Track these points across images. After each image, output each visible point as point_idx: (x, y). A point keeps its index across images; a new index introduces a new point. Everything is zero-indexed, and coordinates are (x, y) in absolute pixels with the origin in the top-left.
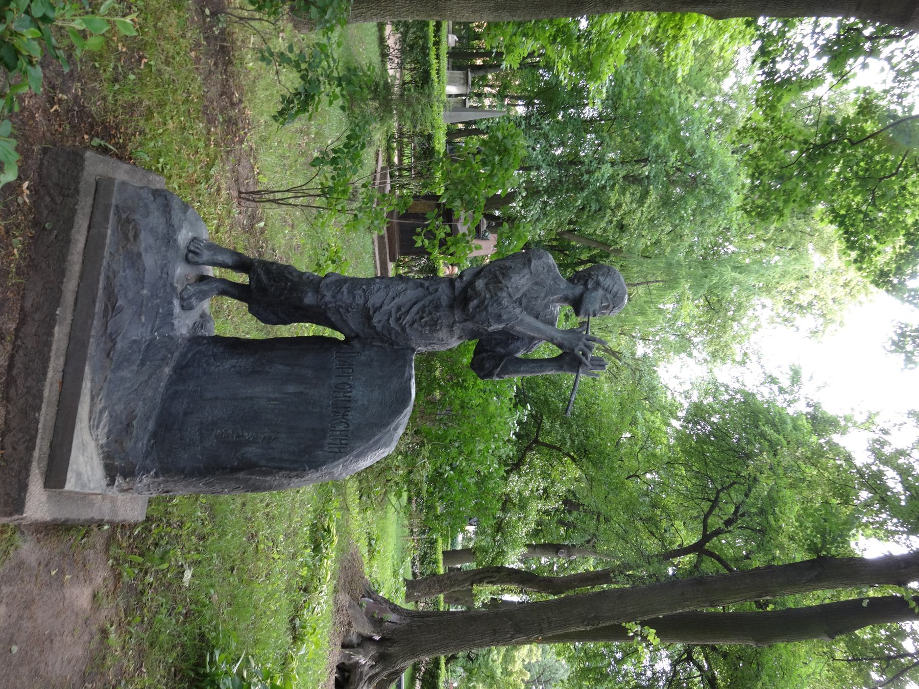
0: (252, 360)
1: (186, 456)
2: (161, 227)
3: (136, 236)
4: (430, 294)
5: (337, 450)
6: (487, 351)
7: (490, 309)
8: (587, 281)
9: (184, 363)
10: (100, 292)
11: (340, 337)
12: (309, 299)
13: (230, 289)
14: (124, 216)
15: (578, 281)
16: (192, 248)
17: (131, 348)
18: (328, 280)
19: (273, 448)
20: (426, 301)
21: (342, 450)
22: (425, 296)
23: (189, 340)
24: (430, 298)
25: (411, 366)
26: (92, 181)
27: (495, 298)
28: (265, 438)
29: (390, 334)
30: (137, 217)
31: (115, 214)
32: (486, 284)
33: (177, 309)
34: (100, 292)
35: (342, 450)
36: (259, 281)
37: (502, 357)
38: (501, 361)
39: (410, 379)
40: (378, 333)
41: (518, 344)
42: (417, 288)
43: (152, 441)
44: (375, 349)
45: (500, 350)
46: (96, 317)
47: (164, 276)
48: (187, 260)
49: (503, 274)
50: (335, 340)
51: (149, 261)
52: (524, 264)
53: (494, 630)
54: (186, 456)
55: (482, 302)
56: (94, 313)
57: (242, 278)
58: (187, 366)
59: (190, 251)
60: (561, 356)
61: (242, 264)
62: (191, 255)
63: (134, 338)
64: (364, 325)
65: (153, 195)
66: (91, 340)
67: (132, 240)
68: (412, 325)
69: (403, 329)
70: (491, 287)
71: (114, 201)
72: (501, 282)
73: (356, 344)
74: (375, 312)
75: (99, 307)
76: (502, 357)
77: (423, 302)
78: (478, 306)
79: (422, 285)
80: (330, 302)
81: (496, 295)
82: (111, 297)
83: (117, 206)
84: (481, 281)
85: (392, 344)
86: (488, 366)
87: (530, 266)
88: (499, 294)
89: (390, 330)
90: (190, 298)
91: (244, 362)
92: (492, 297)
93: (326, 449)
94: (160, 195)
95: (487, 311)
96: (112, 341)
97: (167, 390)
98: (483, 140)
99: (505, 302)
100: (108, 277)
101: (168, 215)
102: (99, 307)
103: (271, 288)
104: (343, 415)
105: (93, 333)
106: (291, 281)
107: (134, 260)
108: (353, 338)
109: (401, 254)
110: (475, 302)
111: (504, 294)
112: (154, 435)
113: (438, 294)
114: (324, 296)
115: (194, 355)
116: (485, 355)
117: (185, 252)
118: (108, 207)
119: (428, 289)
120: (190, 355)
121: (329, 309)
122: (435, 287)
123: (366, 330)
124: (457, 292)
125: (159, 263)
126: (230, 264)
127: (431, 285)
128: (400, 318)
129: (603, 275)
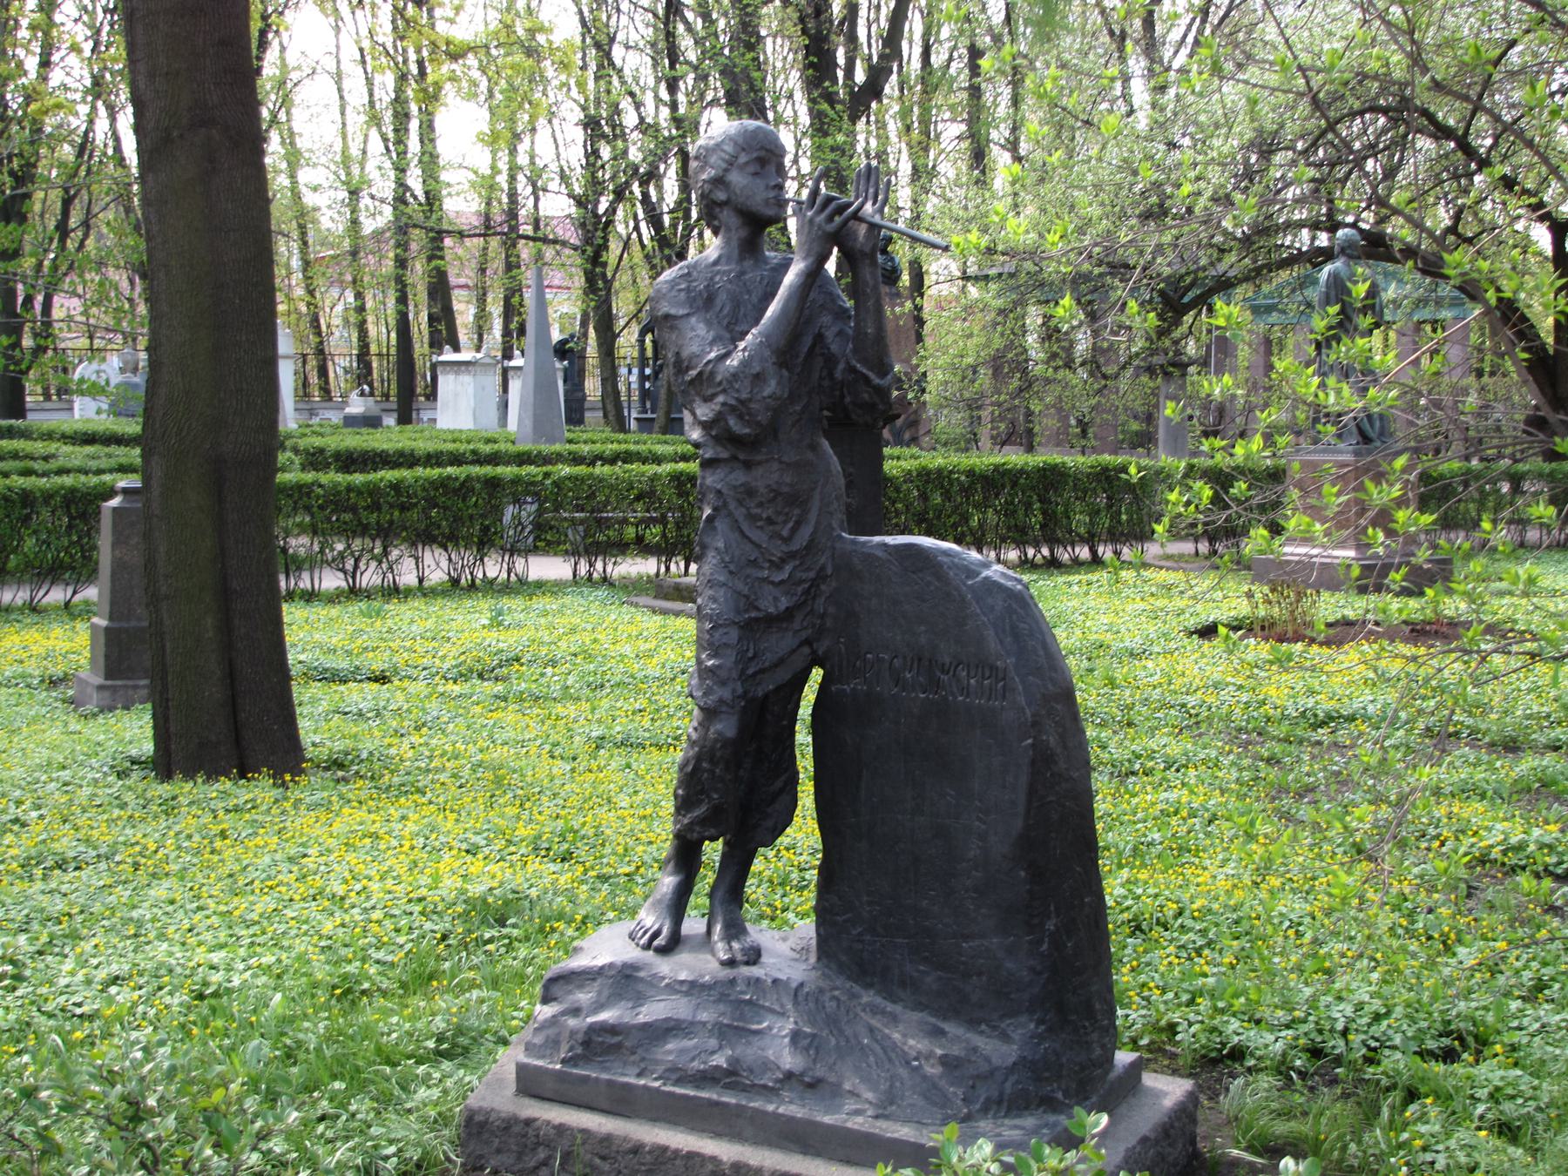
4: (725, 504)
7: (744, 396)
8: (714, 202)
10: (704, 1094)
11: (817, 674)
20: (740, 513)
21: (1001, 675)
22: (730, 514)
24: (732, 505)
25: (864, 543)
29: (802, 581)
31: (575, 1066)
33: (755, 971)
34: (704, 1094)
35: (1001, 675)
39: (885, 545)
42: (715, 529)
43: (983, 1027)
52: (672, 328)
56: (738, 1106)
57: (713, 851)
61: (686, 857)
66: (781, 1110)
69: (792, 555)
74: (758, 609)
75: (729, 1099)
77: (741, 519)
78: (741, 417)
80: (734, 691)
81: (720, 383)
82: (707, 1078)
87: (675, 317)
92: (724, 391)
95: (750, 400)
98: (115, 509)
100: (678, 1082)
102: (729, 1099)
103: (729, 799)
105: (771, 1108)
110: (732, 422)
113: (724, 491)
121: (745, 692)
123: (796, 625)
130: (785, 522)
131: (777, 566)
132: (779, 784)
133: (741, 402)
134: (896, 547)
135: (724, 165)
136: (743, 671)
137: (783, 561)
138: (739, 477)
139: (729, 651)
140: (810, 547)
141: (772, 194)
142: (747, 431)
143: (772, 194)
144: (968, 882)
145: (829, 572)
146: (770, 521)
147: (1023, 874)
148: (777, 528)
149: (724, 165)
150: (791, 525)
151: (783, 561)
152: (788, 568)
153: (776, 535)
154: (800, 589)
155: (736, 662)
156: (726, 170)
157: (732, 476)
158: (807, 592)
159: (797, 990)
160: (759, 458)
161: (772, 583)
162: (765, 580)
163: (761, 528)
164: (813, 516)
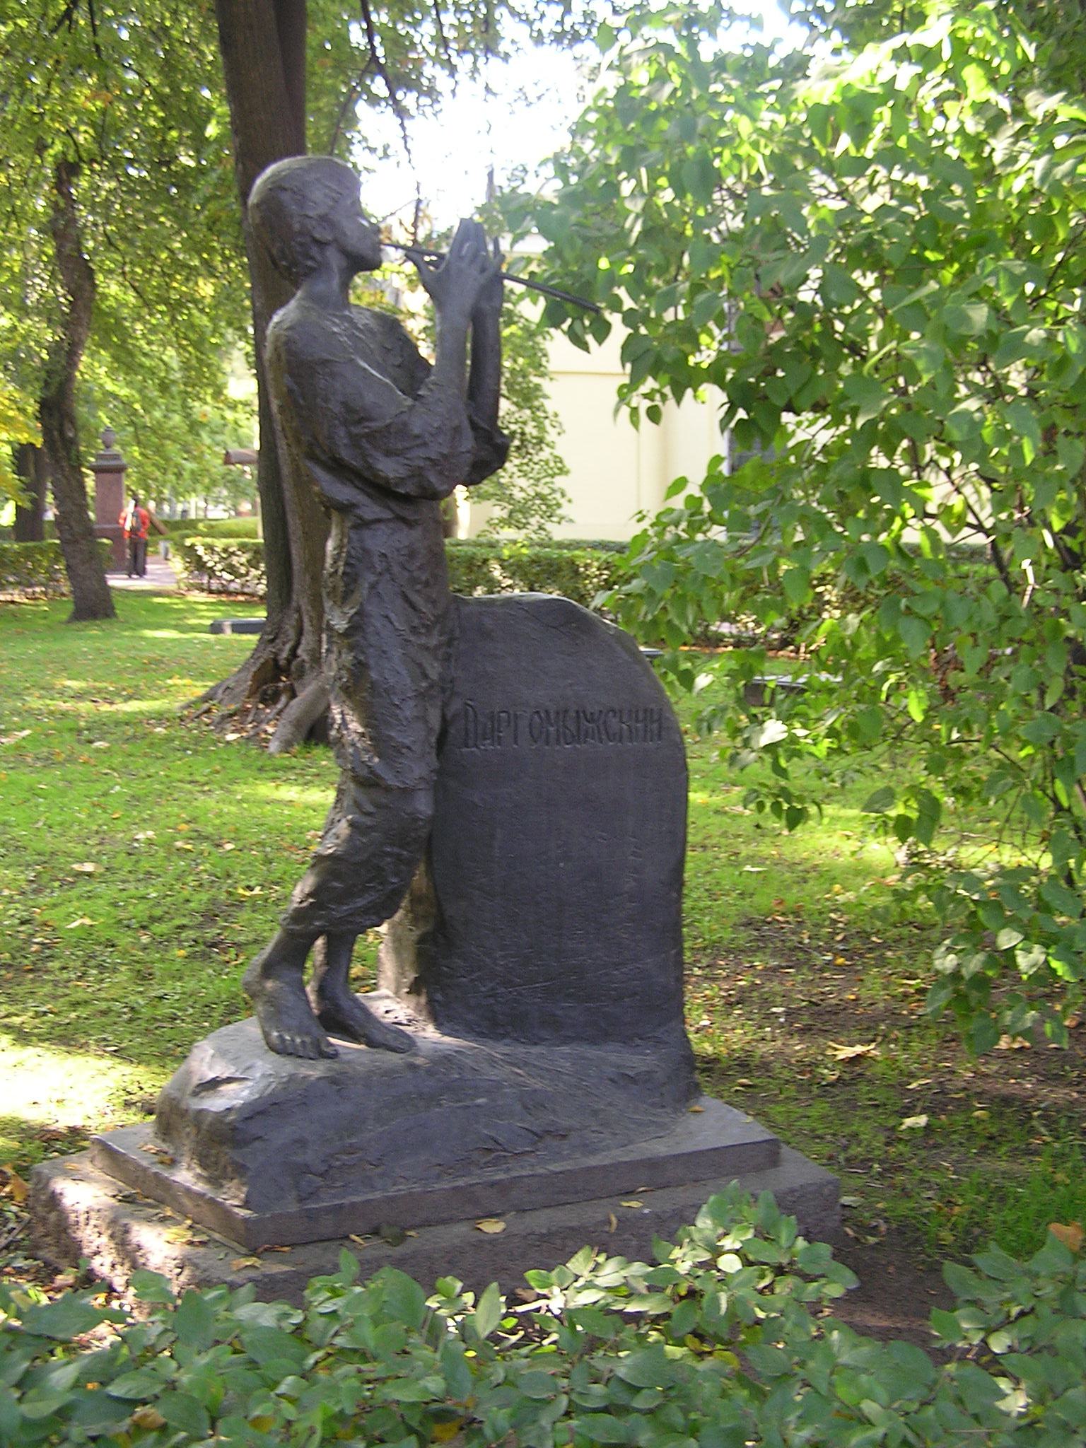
4: (388, 570)
24: (396, 569)
55: (434, 463)
72: (388, 426)
78: (441, 473)
124: (387, 515)
127: (371, 568)
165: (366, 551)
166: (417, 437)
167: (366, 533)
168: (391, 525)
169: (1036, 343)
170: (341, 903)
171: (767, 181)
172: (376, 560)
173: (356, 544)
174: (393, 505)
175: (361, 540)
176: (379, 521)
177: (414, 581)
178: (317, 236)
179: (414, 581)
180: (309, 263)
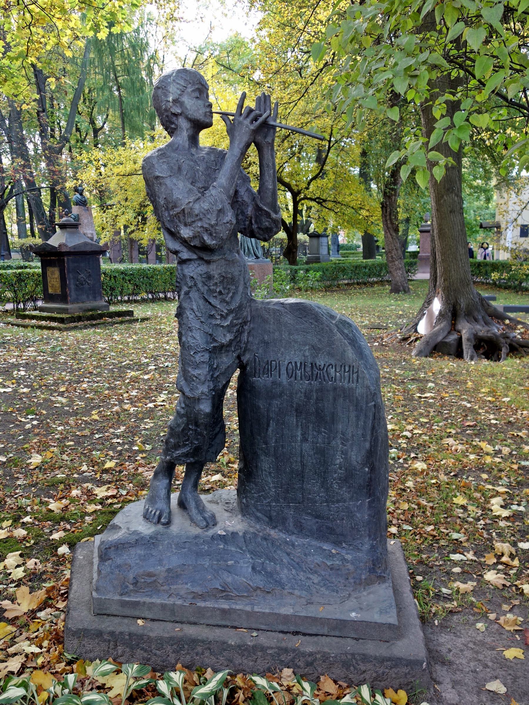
0: (263, 457)
1: (358, 515)
2: (139, 552)
3: (150, 575)
4: (195, 285)
5: (355, 375)
6: (251, 223)
7: (213, 222)
9: (267, 519)
12: (206, 407)
13: (192, 480)
14: (131, 587)
15: (173, 123)
16: (155, 520)
17: (260, 572)
18: (187, 390)
19: (353, 436)
20: (204, 289)
23: (244, 516)
24: (200, 285)
25: (269, 303)
26: (96, 619)
27: (201, 216)
28: (342, 443)
30: (131, 576)
31: (130, 596)
32: (186, 225)
35: (355, 370)
36: (186, 455)
37: (258, 209)
38: (261, 209)
40: (236, 337)
41: (242, 191)
43: (344, 545)
44: (251, 339)
45: (250, 211)
46: (234, 607)
47: (187, 545)
48: (168, 523)
49: (175, 206)
50: (240, 378)
51: (174, 561)
53: (451, 212)
54: (358, 515)
55: (206, 230)
58: (270, 518)
59: (159, 521)
60: (257, 145)
62: (163, 520)
63: (250, 570)
64: (228, 351)
65: (106, 561)
67: (153, 579)
68: (228, 303)
69: (230, 312)
70: (189, 220)
71: (117, 597)
72: (183, 210)
73: (246, 358)
76: (258, 209)
78: (211, 234)
79: (187, 293)
80: (209, 386)
83: (121, 595)
84: (182, 232)
85: (245, 323)
86: (267, 223)
88: (197, 212)
89: (232, 325)
90: (205, 518)
91: (266, 463)
92: (201, 219)
93: (354, 385)
94: (106, 554)
96: (255, 590)
97: (293, 533)
99: (206, 206)
101: (126, 546)
104: (320, 369)
106: (187, 424)
107: (173, 576)
108: (241, 361)
109: (9, 257)
111: (197, 206)
112: (337, 543)
114: (202, 393)
115: (258, 510)
116: (255, 226)
117: (160, 527)
118: (124, 604)
119: (190, 287)
120: (259, 514)
122: (188, 279)
124: (195, 257)
125: (175, 551)
126: (168, 481)
127: (186, 284)
128: (221, 315)
129: (166, 96)
130: (228, 294)
131: (224, 317)
132: (217, 429)
133: (212, 226)
134: (291, 305)
135: (179, 92)
136: (212, 376)
137: (227, 315)
138: (203, 268)
139: (205, 366)
140: (240, 307)
141: (208, 110)
142: (214, 242)
143: (208, 110)
144: (335, 476)
145: (249, 319)
146: (220, 293)
147: (367, 469)
148: (224, 296)
149: (179, 92)
150: (231, 294)
151: (227, 315)
152: (230, 318)
153: (223, 301)
154: (235, 329)
155: (209, 371)
156: (180, 95)
157: (199, 269)
158: (238, 331)
159: (244, 537)
160: (215, 258)
161: (222, 326)
162: (218, 325)
163: (216, 297)
164: (241, 288)
165: (184, 275)
166: (197, 215)
167: (184, 266)
168: (197, 262)
169: (452, 342)
170: (176, 450)
171: (451, 97)
172: (188, 279)
173: (180, 272)
174: (197, 252)
175: (182, 270)
176: (190, 260)
177: (210, 291)
178: (173, 111)
179: (210, 291)
180: (173, 126)
